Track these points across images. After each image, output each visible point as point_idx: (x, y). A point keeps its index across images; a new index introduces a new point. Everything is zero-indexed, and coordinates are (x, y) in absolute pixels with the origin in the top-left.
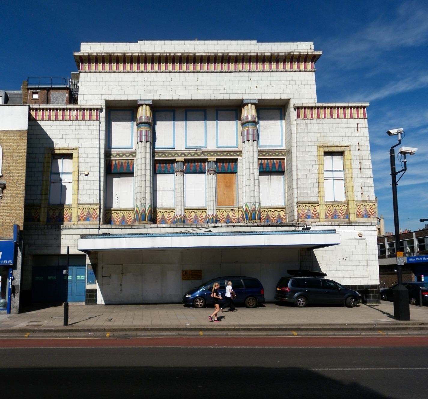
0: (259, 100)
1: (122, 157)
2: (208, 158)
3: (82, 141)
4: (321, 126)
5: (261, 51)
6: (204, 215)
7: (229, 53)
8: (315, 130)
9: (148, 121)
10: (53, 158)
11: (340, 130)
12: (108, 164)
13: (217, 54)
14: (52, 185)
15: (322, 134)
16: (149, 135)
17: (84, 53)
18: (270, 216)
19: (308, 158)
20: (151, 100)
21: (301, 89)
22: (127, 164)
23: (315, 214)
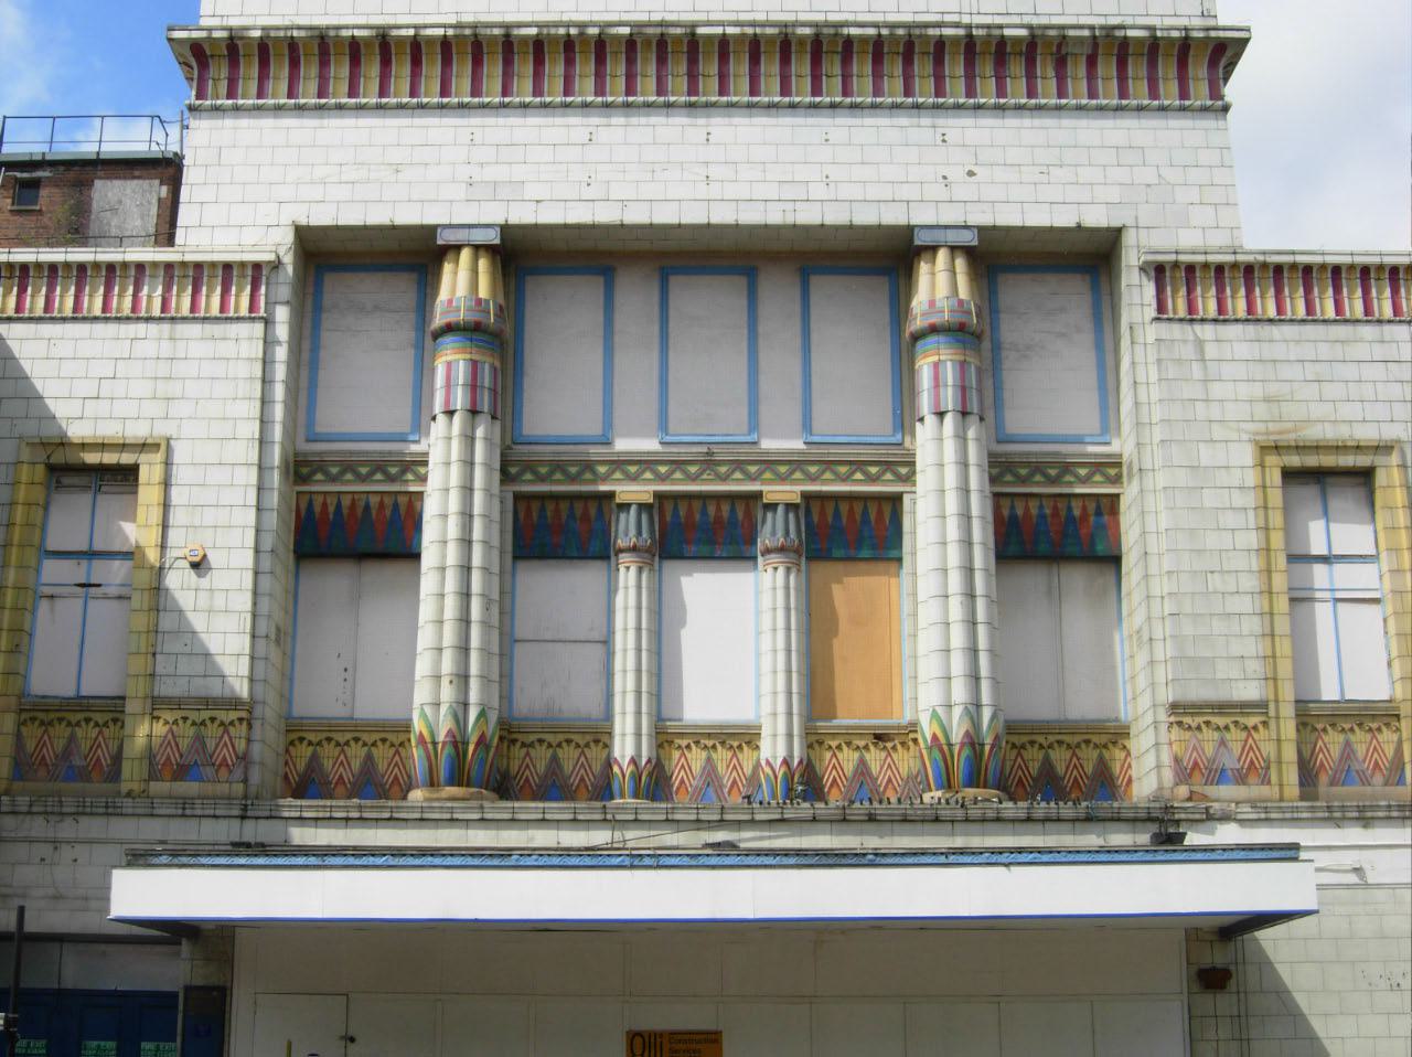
0: (981, 229)
1: (1024, 481)
2: (765, 488)
3: (181, 409)
4: (1269, 351)
5: (988, 20)
6: (747, 759)
7: (847, 24)
8: (1240, 371)
9: (484, 321)
10: (54, 485)
11: (1350, 371)
12: (303, 513)
13: (790, 30)
14: (44, 605)
15: (1273, 389)
16: (974, 386)
17: (210, 30)
18: (1060, 769)
19: (1209, 499)
20: (498, 229)
21: (1169, 184)
22: (388, 513)
23: (1252, 762)
